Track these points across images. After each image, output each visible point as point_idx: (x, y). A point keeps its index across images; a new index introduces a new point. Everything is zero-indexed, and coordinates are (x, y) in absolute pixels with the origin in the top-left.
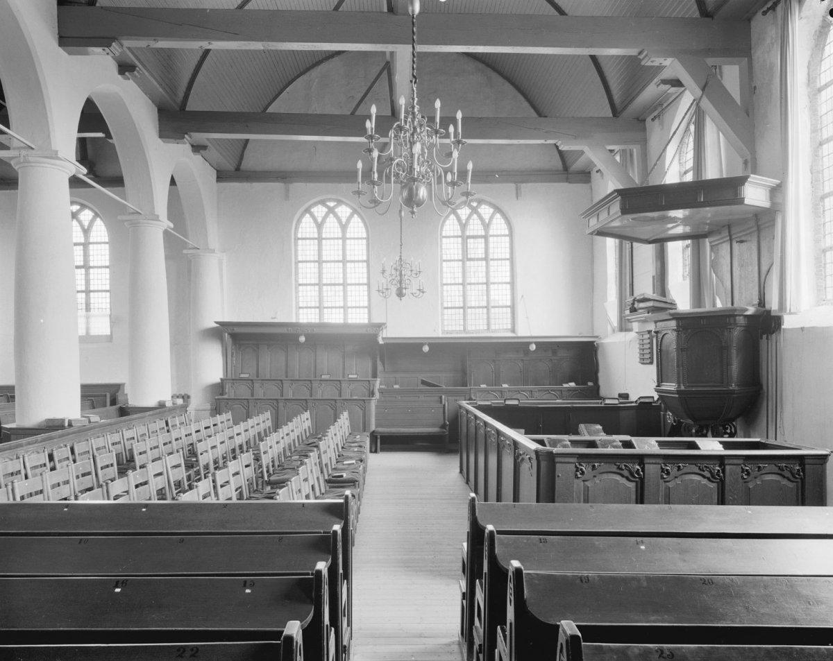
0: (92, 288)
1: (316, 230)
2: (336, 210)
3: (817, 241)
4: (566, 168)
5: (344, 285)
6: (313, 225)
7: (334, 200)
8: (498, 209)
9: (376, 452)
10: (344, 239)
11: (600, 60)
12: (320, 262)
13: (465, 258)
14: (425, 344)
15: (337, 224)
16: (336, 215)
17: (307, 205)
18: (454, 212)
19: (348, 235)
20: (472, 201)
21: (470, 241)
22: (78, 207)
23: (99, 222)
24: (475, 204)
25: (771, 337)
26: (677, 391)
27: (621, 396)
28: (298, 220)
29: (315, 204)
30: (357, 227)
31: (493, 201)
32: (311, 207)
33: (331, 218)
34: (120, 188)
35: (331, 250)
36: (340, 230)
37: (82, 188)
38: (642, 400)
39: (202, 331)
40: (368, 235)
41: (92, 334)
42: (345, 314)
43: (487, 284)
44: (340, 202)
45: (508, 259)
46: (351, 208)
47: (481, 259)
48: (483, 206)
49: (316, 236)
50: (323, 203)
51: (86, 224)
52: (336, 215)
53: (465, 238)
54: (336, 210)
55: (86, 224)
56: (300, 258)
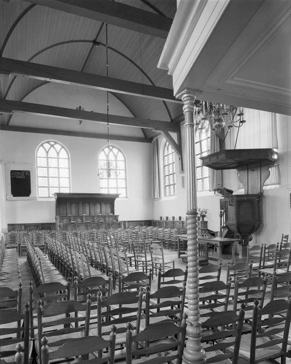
0: (60, 176)
2: (50, 146)
3: (164, 164)
4: (146, 137)
5: (59, 178)
10: (58, 158)
11: (166, 102)
15: (55, 152)
16: (54, 148)
17: (103, 148)
20: (110, 146)
24: (111, 148)
25: (85, 209)
28: (38, 149)
30: (63, 154)
35: (53, 163)
40: (125, 159)
42: (59, 189)
45: (60, 168)
46: (61, 146)
49: (46, 156)
50: (48, 142)
54: (50, 146)
56: (38, 166)
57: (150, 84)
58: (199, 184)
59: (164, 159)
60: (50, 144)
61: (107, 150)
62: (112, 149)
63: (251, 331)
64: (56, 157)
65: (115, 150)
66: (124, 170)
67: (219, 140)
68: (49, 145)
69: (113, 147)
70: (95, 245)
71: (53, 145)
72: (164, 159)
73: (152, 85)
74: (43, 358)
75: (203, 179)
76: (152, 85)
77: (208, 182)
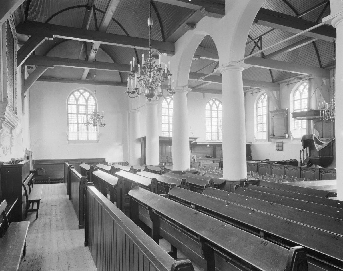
1: (167, 105)
6: (166, 103)
7: (83, 89)
8: (220, 102)
9: (334, 172)
12: (78, 113)
13: (211, 117)
14: (208, 144)
16: (84, 96)
18: (165, 98)
19: (213, 109)
21: (213, 112)
22: (83, 91)
23: (91, 97)
26: (321, 159)
27: (266, 160)
29: (75, 91)
31: (219, 99)
32: (74, 92)
33: (82, 96)
34: (220, 95)
36: (75, 101)
37: (88, 84)
38: (290, 160)
39: (136, 140)
41: (89, 140)
43: (211, 125)
44: (86, 91)
46: (89, 92)
47: (216, 117)
48: (216, 101)
49: (85, 104)
50: (78, 90)
51: (77, 97)
52: (84, 96)
53: (211, 110)
55: (77, 97)
57: (125, 34)
58: (266, 120)
59: (294, 104)
60: (80, 92)
61: (211, 102)
62: (215, 101)
63: (254, 42)
64: (216, 109)
65: (87, 94)
66: (88, 139)
67: (35, 50)
68: (78, 93)
69: (216, 99)
70: (316, 245)
71: (83, 92)
72: (294, 104)
73: (127, 35)
74: (279, 68)
75: (262, 115)
76: (127, 35)
77: (266, 118)
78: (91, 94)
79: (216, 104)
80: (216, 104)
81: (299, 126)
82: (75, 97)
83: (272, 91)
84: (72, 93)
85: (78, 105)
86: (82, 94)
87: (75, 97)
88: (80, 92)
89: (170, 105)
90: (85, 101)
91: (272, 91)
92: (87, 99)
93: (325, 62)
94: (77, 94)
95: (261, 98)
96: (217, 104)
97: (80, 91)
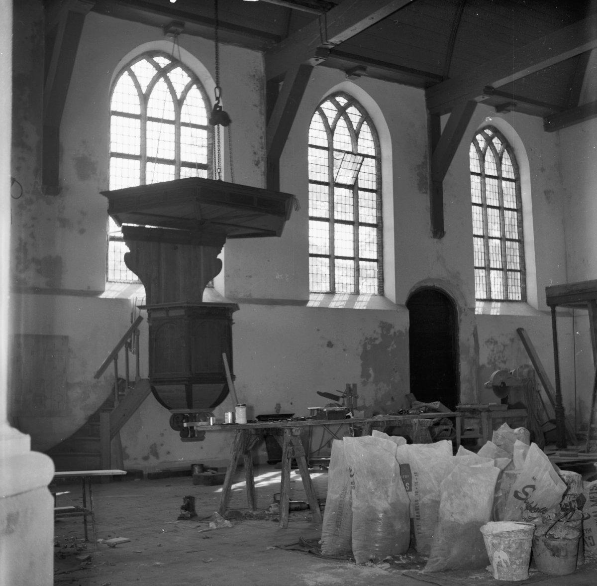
29: (187, 69)
33: (161, 84)
50: (149, 55)
60: (156, 66)
68: (150, 66)
78: (196, 80)
79: (494, 149)
80: (494, 149)
81: (349, 282)
82: (138, 86)
83: (320, 301)
84: (127, 67)
85: (330, 149)
86: (162, 73)
87: (138, 86)
88: (156, 66)
89: (336, 137)
90: (137, 100)
91: (320, 301)
92: (179, 97)
93: (15, 183)
94: (144, 70)
95: (304, 432)
96: (179, 90)
97: (156, 59)
